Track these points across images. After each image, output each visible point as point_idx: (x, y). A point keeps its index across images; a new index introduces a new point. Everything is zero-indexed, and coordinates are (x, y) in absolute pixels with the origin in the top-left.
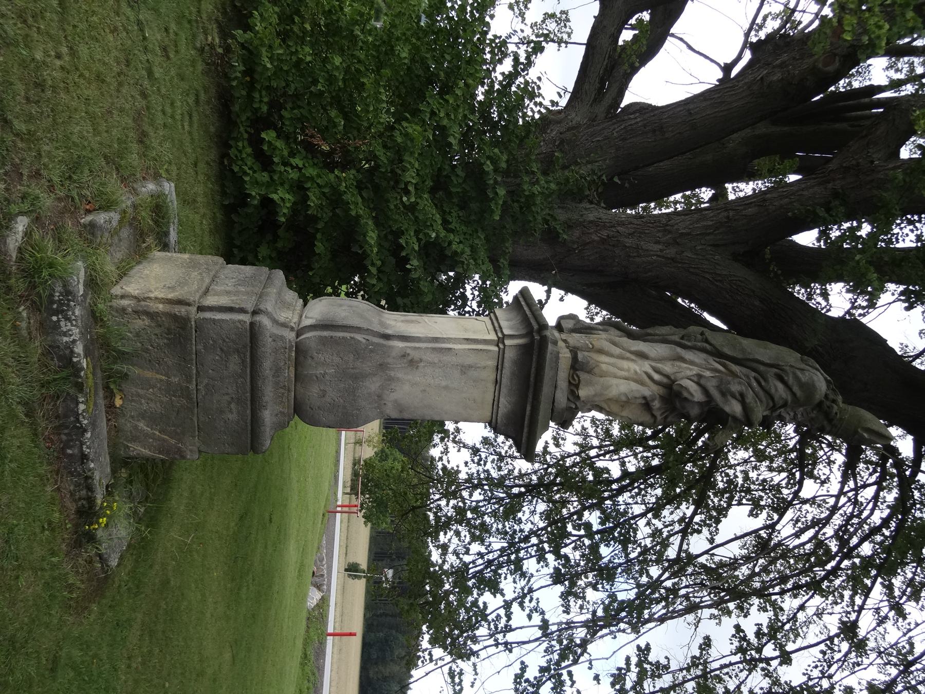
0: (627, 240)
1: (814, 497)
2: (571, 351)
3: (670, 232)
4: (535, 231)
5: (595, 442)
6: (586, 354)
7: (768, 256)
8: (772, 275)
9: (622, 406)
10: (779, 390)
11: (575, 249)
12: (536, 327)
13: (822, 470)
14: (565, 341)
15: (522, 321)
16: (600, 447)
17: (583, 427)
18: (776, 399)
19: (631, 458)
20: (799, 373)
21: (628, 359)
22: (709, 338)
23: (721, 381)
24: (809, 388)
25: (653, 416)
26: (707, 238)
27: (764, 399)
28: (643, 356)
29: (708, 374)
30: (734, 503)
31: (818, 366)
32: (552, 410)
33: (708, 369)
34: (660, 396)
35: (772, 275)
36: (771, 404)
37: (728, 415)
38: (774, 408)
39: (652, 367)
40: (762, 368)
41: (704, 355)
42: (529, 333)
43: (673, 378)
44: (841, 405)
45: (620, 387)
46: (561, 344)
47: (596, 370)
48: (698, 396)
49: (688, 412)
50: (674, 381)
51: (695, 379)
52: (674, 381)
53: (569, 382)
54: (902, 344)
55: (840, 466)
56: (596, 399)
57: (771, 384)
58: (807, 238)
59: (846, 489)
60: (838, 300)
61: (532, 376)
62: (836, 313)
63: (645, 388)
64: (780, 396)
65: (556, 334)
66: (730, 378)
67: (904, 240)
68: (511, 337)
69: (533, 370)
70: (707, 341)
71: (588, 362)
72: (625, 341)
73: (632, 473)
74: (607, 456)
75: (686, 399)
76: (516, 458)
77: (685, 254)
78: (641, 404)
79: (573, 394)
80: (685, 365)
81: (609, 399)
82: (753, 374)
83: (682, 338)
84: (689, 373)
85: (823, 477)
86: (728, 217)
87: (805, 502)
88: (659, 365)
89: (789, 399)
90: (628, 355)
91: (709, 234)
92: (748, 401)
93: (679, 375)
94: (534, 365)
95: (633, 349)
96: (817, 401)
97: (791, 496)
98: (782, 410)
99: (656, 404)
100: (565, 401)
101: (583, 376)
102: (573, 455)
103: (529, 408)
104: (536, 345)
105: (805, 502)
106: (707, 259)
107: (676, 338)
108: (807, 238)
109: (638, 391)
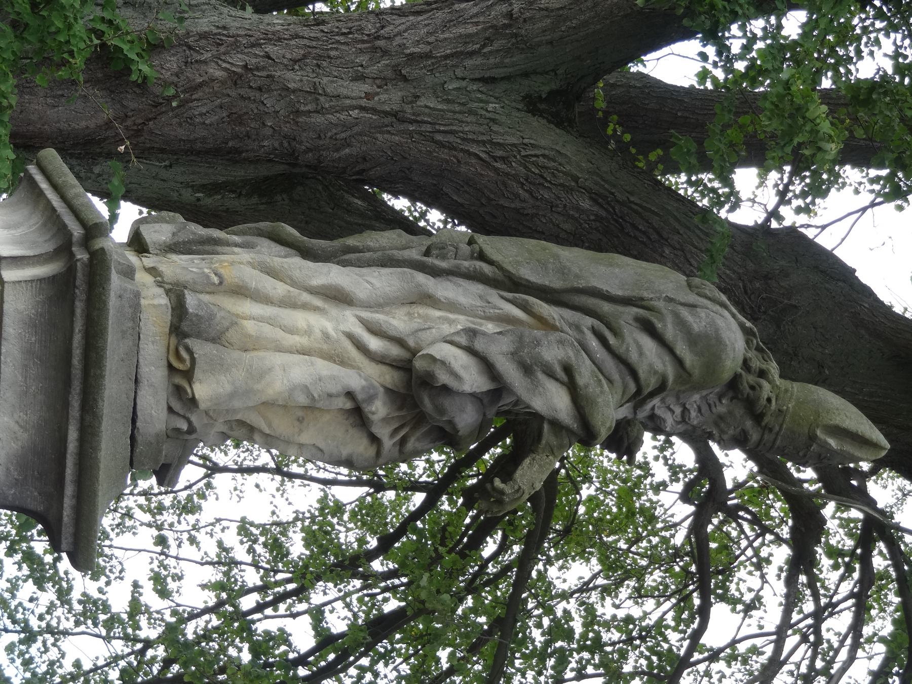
0: (289, 75)
1: (733, 643)
2: (168, 292)
3: (385, 53)
4: (71, 53)
5: (252, 577)
6: (206, 298)
7: (601, 104)
8: (612, 145)
9: (300, 420)
11: (169, 100)
12: (77, 231)
13: (745, 581)
15: (44, 225)
16: (262, 589)
17: (220, 544)
18: (642, 375)
19: (339, 605)
20: (685, 313)
21: (305, 307)
24: (709, 345)
25: (374, 440)
26: (469, 63)
27: (616, 377)
28: (338, 297)
29: (490, 328)
30: (569, 675)
31: (724, 298)
32: (133, 438)
33: (489, 318)
35: (612, 145)
36: (632, 388)
37: (538, 417)
38: (639, 398)
40: (606, 307)
41: (478, 288)
42: (64, 249)
43: (411, 343)
44: (778, 381)
45: (291, 373)
46: (143, 278)
47: (232, 335)
48: (472, 380)
49: (451, 422)
50: (414, 352)
51: (463, 340)
52: (414, 352)
53: (170, 367)
55: (781, 569)
56: (237, 404)
58: (676, 65)
59: (795, 617)
60: (753, 196)
61: (76, 361)
62: (746, 216)
64: (651, 365)
65: (132, 258)
66: (538, 333)
67: (871, 53)
71: (212, 316)
73: (342, 635)
74: (282, 607)
75: (446, 389)
76: (66, 633)
77: (422, 102)
79: (182, 397)
80: (438, 313)
82: (589, 321)
83: (427, 253)
84: (447, 329)
85: (748, 597)
86: (510, 15)
87: (714, 656)
89: (670, 372)
90: (306, 297)
91: (471, 54)
93: (426, 336)
94: (79, 325)
96: (727, 376)
97: (686, 643)
98: (656, 401)
99: (379, 409)
100: (163, 414)
101: (201, 348)
102: (199, 615)
103: (73, 435)
104: (79, 275)
105: (714, 656)
106: (471, 112)
107: (414, 254)
108: (676, 65)
109: (333, 378)
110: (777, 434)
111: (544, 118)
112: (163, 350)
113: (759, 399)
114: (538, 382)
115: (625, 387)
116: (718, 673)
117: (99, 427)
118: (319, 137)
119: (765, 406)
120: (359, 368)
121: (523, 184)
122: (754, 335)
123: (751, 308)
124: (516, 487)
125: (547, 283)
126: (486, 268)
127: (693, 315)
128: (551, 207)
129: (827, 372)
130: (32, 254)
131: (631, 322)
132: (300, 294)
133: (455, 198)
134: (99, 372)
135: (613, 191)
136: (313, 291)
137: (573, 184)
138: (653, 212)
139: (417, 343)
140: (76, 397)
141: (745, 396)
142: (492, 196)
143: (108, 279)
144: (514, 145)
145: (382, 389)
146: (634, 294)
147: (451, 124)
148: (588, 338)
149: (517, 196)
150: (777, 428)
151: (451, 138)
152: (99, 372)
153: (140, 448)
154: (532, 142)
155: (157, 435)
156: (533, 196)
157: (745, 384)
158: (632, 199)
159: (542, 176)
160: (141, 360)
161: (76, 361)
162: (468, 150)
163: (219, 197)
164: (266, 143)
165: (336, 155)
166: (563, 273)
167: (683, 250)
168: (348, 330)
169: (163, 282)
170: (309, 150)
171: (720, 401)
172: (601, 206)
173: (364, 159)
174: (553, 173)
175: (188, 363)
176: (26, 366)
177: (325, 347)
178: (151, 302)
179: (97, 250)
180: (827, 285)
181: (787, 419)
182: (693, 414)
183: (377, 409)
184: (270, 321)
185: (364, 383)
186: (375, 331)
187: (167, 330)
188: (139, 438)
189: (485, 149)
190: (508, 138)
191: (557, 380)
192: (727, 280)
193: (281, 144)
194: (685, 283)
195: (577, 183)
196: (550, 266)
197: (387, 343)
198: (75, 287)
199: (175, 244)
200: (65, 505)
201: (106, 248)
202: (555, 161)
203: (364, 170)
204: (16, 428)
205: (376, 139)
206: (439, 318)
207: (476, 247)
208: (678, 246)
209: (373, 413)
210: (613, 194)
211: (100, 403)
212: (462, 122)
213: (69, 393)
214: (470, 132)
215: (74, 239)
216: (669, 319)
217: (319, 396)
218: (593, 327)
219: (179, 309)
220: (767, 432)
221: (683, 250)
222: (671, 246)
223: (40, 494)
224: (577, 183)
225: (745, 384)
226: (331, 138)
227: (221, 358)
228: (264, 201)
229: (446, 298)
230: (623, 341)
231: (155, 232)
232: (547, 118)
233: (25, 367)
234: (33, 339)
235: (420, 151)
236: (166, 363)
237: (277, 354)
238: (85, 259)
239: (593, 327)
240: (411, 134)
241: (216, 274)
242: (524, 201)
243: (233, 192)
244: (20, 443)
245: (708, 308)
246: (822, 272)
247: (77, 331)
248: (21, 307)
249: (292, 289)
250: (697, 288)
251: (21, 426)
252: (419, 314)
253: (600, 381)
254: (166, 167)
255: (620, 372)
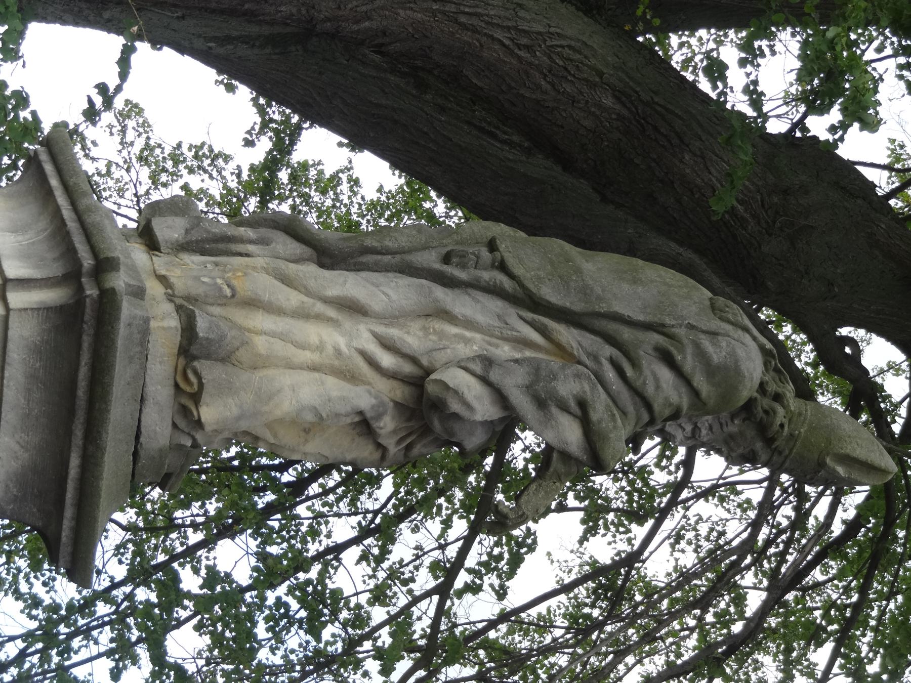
2: (179, 308)
6: (216, 310)
9: (307, 431)
10: (663, 385)
12: (87, 262)
14: (163, 280)
18: (657, 407)
20: (706, 344)
21: (319, 318)
22: (511, 262)
23: (536, 369)
25: (379, 446)
27: (630, 409)
28: (353, 308)
29: (505, 351)
32: (136, 454)
34: (396, 403)
36: (646, 417)
39: (376, 335)
42: (72, 276)
43: (425, 362)
47: (243, 355)
53: (177, 385)
54: (893, 141)
57: (647, 372)
61: (81, 392)
63: (360, 390)
64: (666, 399)
65: (139, 254)
68: (24, 283)
69: (83, 372)
70: (502, 267)
71: (222, 337)
72: (310, 272)
75: (456, 416)
78: (351, 424)
80: (454, 330)
81: (281, 421)
82: (608, 351)
84: (464, 351)
88: (394, 332)
90: (320, 307)
92: (594, 416)
93: (441, 357)
94: (85, 358)
95: (332, 292)
99: (387, 425)
100: (169, 429)
101: (210, 371)
103: (75, 462)
104: (89, 311)
109: (343, 398)
110: (786, 457)
111: (573, 4)
112: (171, 370)
113: (772, 425)
114: (552, 415)
115: (638, 418)
116: (695, 516)
117: (102, 458)
118: (339, 8)
119: (778, 432)
120: (369, 384)
121: (545, 75)
122: (773, 357)
123: (767, 222)
124: (520, 513)
125: (568, 304)
126: (507, 283)
127: (714, 344)
128: (573, 102)
129: (836, 290)
130: (39, 277)
131: (650, 352)
132: (314, 305)
133: (475, 81)
134: (104, 406)
135: (638, 89)
136: (327, 301)
137: (597, 79)
138: (677, 115)
139: (431, 363)
140: (80, 426)
141: (758, 420)
142: (513, 84)
143: (118, 309)
144: (540, 33)
145: (391, 404)
146: (656, 319)
147: (477, 6)
148: (605, 369)
149: (539, 87)
150: (787, 452)
151: (475, 21)
152: (104, 406)
153: (142, 461)
154: (558, 31)
155: (161, 450)
156: (555, 88)
157: (759, 408)
158: (656, 100)
159: (566, 69)
160: (147, 380)
161: (81, 392)
162: (492, 36)
163: (232, 47)
164: (283, 8)
165: (355, 27)
166: (585, 294)
167: (703, 158)
168: (361, 347)
169: (173, 295)
170: (328, 19)
171: (732, 420)
172: (624, 105)
173: (384, 33)
174: (577, 66)
175: (196, 387)
176: (29, 390)
177: (336, 363)
178: (160, 324)
179: (108, 290)
180: (846, 203)
181: (798, 443)
182: (704, 432)
183: (385, 425)
184: (282, 337)
185: (374, 401)
186: (388, 346)
187: (176, 351)
188: (142, 453)
189: (510, 36)
190: (534, 25)
191: (570, 413)
192: (745, 192)
193: (299, 11)
194: (708, 303)
195: (601, 77)
196: (573, 284)
197: (400, 360)
198: (83, 321)
199: (187, 243)
200: (64, 527)
201: (117, 289)
202: (580, 53)
203: (382, 45)
204: (17, 448)
205: (398, 14)
206: (455, 335)
207: (497, 254)
208: (699, 153)
209: (381, 428)
210: (637, 92)
211: (104, 435)
212: (488, 4)
213: (73, 422)
214: (495, 15)
215: (84, 270)
216: (689, 350)
217: (328, 416)
218: (611, 357)
219: (189, 329)
220: (776, 454)
221: (703, 158)
222: (691, 151)
223: (39, 510)
224: (601, 77)
225: (759, 408)
226: (351, 9)
227: (230, 382)
228: (277, 51)
229: (463, 316)
230: (641, 373)
231: (167, 227)
232: (576, 5)
233: (29, 390)
234: (38, 364)
235: (442, 31)
236: (172, 382)
237: (287, 371)
238: (95, 296)
239: (611, 357)
240: (434, 13)
241: (229, 286)
242: (546, 93)
243: (247, 43)
244: (20, 463)
245: (729, 336)
246: (842, 188)
247: (83, 363)
248: (26, 333)
249: (305, 299)
250: (721, 311)
251: (22, 447)
252: (434, 330)
253: (614, 415)
254: (178, 17)
255: (635, 404)
